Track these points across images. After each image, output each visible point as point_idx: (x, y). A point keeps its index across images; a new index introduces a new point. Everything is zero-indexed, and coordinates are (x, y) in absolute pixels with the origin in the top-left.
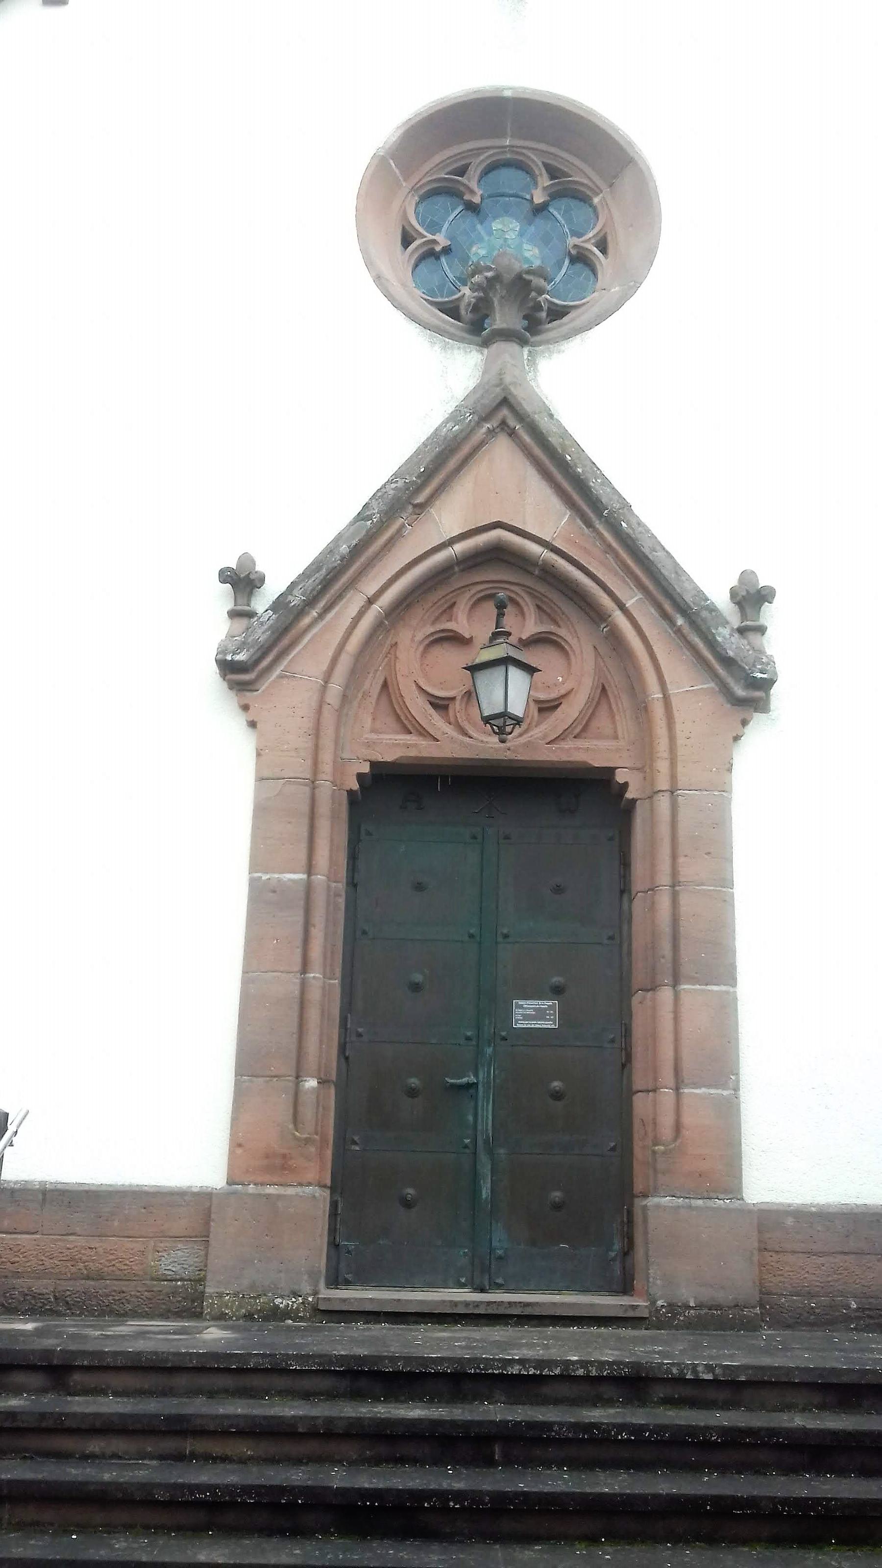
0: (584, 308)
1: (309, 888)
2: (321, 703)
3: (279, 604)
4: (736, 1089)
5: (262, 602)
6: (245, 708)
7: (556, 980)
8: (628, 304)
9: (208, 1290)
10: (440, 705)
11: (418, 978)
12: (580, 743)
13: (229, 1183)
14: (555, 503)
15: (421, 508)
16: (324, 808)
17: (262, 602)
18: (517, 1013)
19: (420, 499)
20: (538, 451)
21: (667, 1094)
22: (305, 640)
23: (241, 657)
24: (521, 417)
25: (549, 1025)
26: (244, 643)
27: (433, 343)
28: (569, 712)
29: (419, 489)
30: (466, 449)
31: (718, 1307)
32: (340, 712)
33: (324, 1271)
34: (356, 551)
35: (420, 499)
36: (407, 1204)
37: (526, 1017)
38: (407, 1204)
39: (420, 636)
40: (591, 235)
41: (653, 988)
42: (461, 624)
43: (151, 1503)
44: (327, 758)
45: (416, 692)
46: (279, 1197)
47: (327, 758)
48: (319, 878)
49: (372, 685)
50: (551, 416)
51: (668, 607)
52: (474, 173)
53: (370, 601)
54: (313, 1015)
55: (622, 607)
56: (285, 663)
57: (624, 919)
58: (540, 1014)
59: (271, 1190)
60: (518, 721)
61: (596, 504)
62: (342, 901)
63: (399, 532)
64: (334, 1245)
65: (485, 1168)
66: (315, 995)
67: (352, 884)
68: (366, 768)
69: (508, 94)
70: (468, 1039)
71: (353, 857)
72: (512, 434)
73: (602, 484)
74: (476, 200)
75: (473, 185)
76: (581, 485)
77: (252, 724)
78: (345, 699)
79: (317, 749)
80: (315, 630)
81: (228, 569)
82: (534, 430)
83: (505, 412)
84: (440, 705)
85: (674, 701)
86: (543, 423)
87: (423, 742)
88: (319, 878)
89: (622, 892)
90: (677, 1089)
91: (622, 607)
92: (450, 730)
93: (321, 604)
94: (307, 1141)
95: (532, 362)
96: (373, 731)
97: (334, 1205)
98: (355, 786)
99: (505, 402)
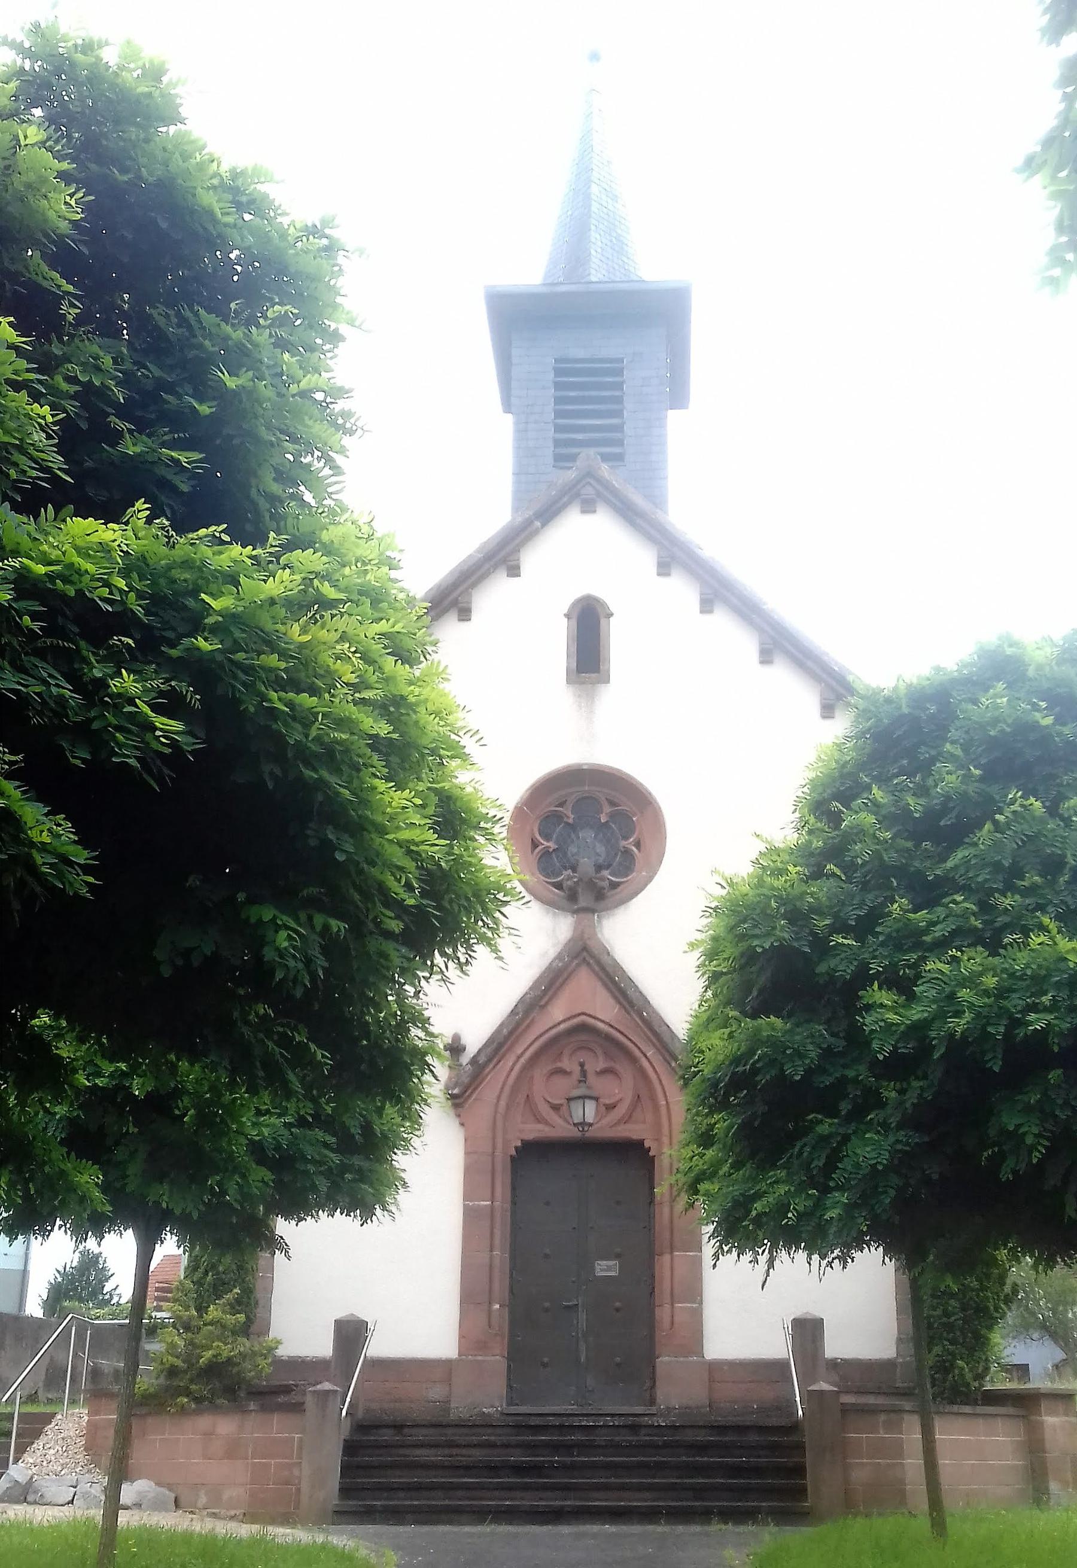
0: (626, 884)
1: (492, 1207)
2: (496, 1112)
3: (474, 1061)
4: (701, 1303)
5: (465, 1059)
6: (459, 1116)
7: (618, 1250)
8: (649, 887)
9: (452, 1406)
10: (556, 1108)
11: (547, 1251)
12: (628, 1126)
13: (460, 1354)
14: (612, 1001)
15: (543, 1007)
16: (499, 1167)
17: (465, 1059)
18: (598, 1268)
19: (543, 1003)
20: (601, 974)
21: (667, 1307)
22: (487, 1080)
23: (456, 1091)
24: (593, 956)
25: (613, 1274)
26: (457, 1082)
27: (548, 913)
28: (621, 1110)
29: (541, 998)
30: (565, 975)
31: (689, 1408)
32: (505, 1117)
33: (505, 1396)
34: (511, 1033)
35: (543, 1003)
36: (545, 1365)
37: (602, 1270)
38: (545, 1365)
39: (545, 1072)
40: (631, 840)
41: (661, 1254)
42: (566, 1064)
43: (444, 1467)
44: (499, 1145)
45: (543, 1102)
46: (484, 1361)
47: (499, 1145)
48: (497, 1204)
49: (521, 1098)
50: (608, 954)
51: (668, 1058)
52: (569, 806)
53: (519, 1057)
54: (610, 286)
55: (645, 1056)
56: (477, 1092)
57: (651, 1217)
58: (609, 1269)
59: (480, 1358)
60: (591, 1125)
61: (631, 1003)
62: (509, 1214)
63: (533, 1021)
64: (510, 1387)
65: (583, 1347)
66: (497, 1262)
67: (514, 1203)
68: (519, 1144)
69: (585, 767)
70: (574, 1282)
71: (514, 1189)
72: (588, 964)
73: (635, 991)
74: (571, 821)
75: (569, 814)
76: (623, 993)
77: (462, 1124)
78: (508, 1107)
79: (518, 535)
80: (492, 1074)
81: (448, 1044)
82: (599, 962)
83: (585, 954)
84: (556, 1108)
85: (671, 1106)
86: (604, 959)
87: (547, 1129)
88: (497, 1204)
89: (650, 1203)
90: (672, 1305)
91: (645, 1056)
92: (560, 1121)
93: (495, 1060)
94: (496, 1335)
95: (600, 922)
96: (523, 1123)
97: (509, 1366)
98: (514, 1153)
99: (585, 948)
